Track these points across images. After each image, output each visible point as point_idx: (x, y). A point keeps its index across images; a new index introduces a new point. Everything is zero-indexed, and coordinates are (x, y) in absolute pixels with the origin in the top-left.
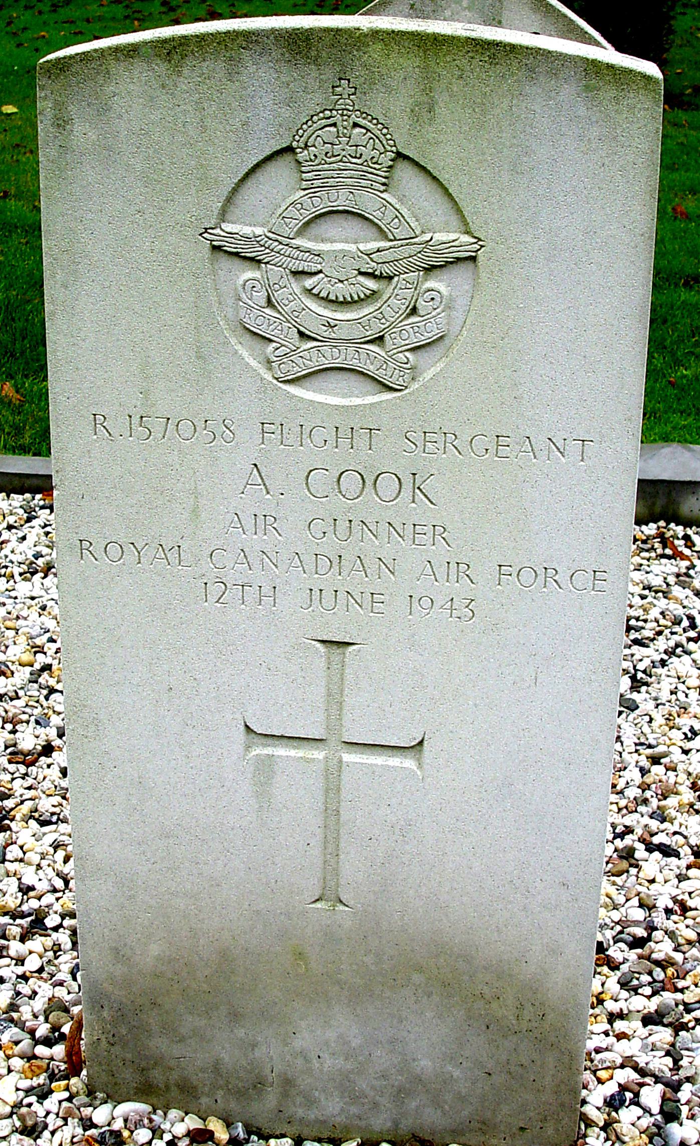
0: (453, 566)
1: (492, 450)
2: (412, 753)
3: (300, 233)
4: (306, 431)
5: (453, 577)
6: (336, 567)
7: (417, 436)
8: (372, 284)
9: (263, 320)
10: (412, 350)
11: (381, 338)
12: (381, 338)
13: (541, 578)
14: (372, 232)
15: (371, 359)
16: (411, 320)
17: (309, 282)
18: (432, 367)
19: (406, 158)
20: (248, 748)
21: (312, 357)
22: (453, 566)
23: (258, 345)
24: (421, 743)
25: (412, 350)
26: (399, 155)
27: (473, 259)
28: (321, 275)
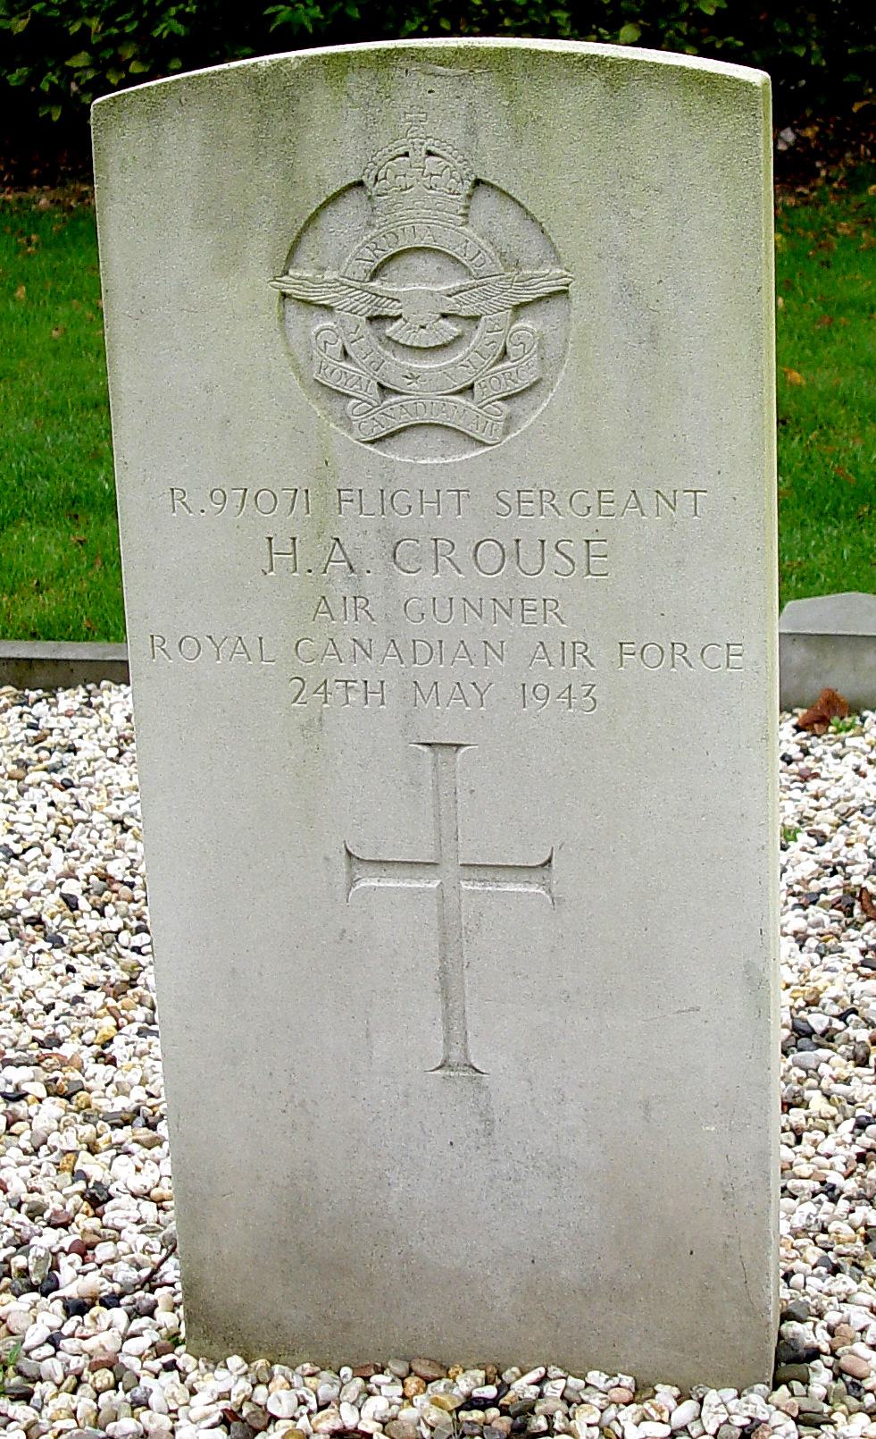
0: (350, 600)
1: (594, 510)
2: (536, 876)
3: (374, 275)
4: (388, 496)
5: (351, 617)
6: (436, 657)
7: (510, 496)
8: (453, 329)
9: (338, 374)
10: (503, 399)
11: (472, 387)
12: (472, 387)
13: (667, 656)
14: (449, 267)
15: (460, 411)
16: (499, 367)
17: (390, 330)
18: (532, 416)
19: (483, 182)
20: (352, 883)
21: (396, 413)
22: (350, 600)
23: (337, 405)
24: (549, 861)
25: (503, 399)
26: (478, 182)
27: (566, 292)
28: (400, 321)
